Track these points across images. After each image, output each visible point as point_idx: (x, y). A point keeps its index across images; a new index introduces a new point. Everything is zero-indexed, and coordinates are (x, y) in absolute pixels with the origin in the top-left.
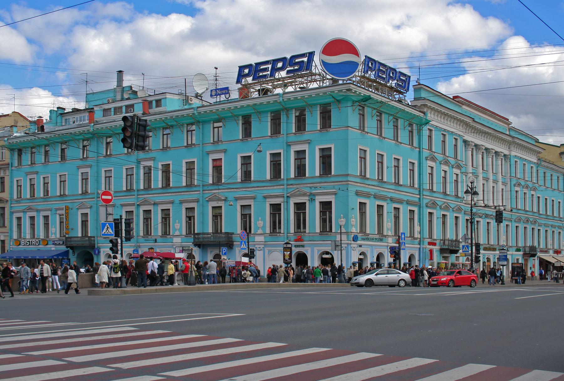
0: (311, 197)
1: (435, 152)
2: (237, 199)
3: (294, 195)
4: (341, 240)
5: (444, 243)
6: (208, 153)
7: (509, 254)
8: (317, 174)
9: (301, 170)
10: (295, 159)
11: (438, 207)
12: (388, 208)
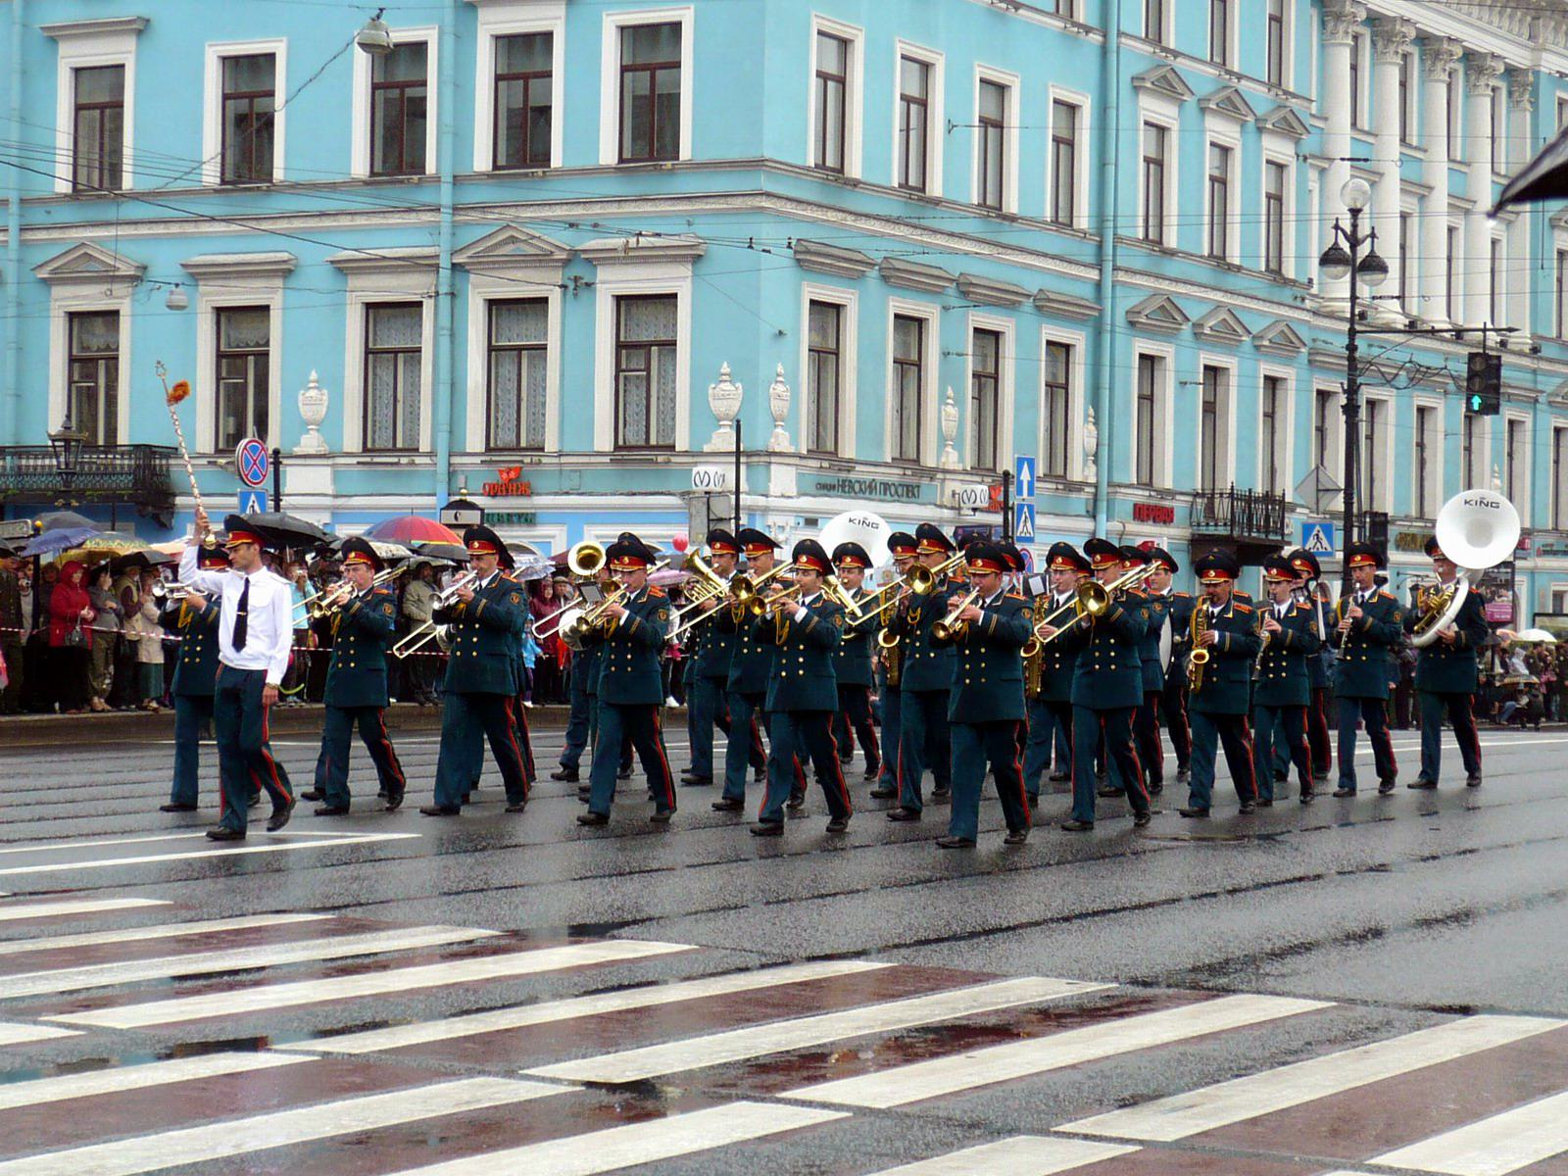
0: (576, 270)
1: (1176, 54)
2: (198, 274)
3: (487, 262)
4: (738, 492)
5: (1210, 509)
6: (54, 36)
7: (1524, 570)
8: (608, 155)
9: (525, 135)
10: (498, 78)
11: (1186, 328)
12: (948, 333)
